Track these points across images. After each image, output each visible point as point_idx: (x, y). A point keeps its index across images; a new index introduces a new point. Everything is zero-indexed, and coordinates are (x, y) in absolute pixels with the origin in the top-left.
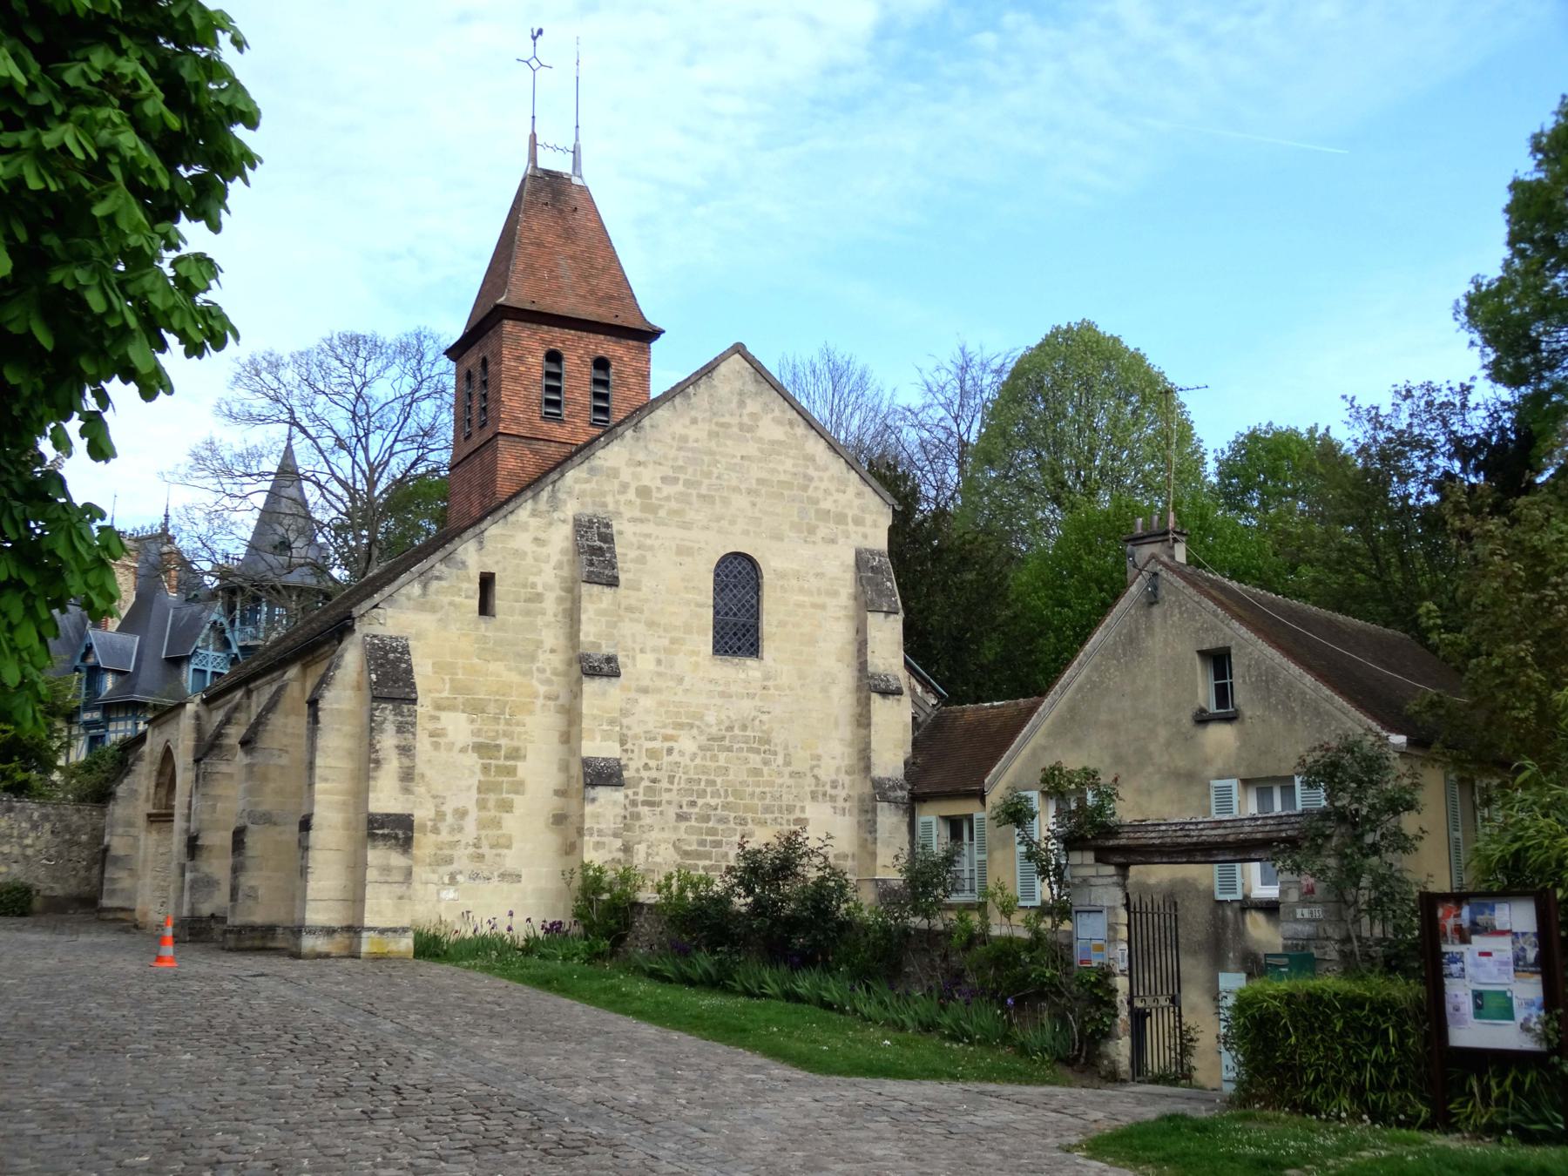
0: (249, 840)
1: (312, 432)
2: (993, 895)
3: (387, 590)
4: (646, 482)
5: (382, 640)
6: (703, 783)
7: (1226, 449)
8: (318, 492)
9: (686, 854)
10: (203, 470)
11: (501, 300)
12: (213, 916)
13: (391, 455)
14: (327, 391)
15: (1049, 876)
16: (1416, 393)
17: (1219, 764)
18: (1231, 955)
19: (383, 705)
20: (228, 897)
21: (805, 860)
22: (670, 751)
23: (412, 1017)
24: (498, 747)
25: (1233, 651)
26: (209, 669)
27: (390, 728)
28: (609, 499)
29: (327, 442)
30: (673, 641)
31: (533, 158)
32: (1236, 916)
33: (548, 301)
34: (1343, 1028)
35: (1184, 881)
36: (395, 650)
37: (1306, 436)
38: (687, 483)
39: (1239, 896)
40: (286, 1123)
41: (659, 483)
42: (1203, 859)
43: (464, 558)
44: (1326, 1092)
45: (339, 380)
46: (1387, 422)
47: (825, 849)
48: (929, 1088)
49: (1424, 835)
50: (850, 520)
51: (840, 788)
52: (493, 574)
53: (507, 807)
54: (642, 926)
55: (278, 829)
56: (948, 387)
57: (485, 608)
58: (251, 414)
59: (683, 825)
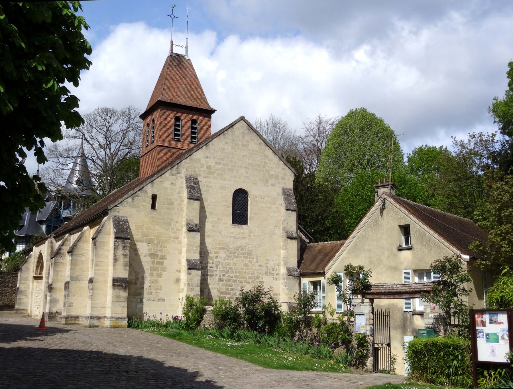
0: (70, 286)
1: (91, 142)
2: (327, 309)
3: (120, 200)
4: (210, 164)
5: (118, 218)
6: (228, 269)
7: (411, 154)
8: (93, 163)
9: (222, 293)
10: (52, 155)
11: (159, 99)
12: (57, 312)
13: (119, 151)
14: (96, 128)
15: (346, 302)
16: (477, 136)
17: (405, 264)
18: (409, 330)
19: (118, 240)
20: (63, 306)
21: (263, 296)
22: (217, 257)
23: (129, 348)
24: (157, 255)
25: (411, 226)
26: (52, 225)
27: (120, 248)
28: (197, 170)
29: (96, 146)
30: (218, 219)
31: (172, 50)
32: (410, 316)
33: (176, 99)
34: (444, 355)
35: (393, 304)
36: (122, 221)
37: (439, 149)
38: (224, 165)
39: (411, 310)
40: (90, 382)
41: (214, 164)
42: (398, 297)
43: (147, 189)
44: (438, 376)
45: (101, 124)
46: (466, 146)
47: (270, 292)
48: (305, 373)
49: (472, 290)
50: (280, 178)
51: (275, 271)
52: (157, 195)
53: (160, 276)
54: (207, 318)
55: (81, 282)
56: (314, 130)
57: (153, 207)
58: (70, 136)
59: (221, 283)
